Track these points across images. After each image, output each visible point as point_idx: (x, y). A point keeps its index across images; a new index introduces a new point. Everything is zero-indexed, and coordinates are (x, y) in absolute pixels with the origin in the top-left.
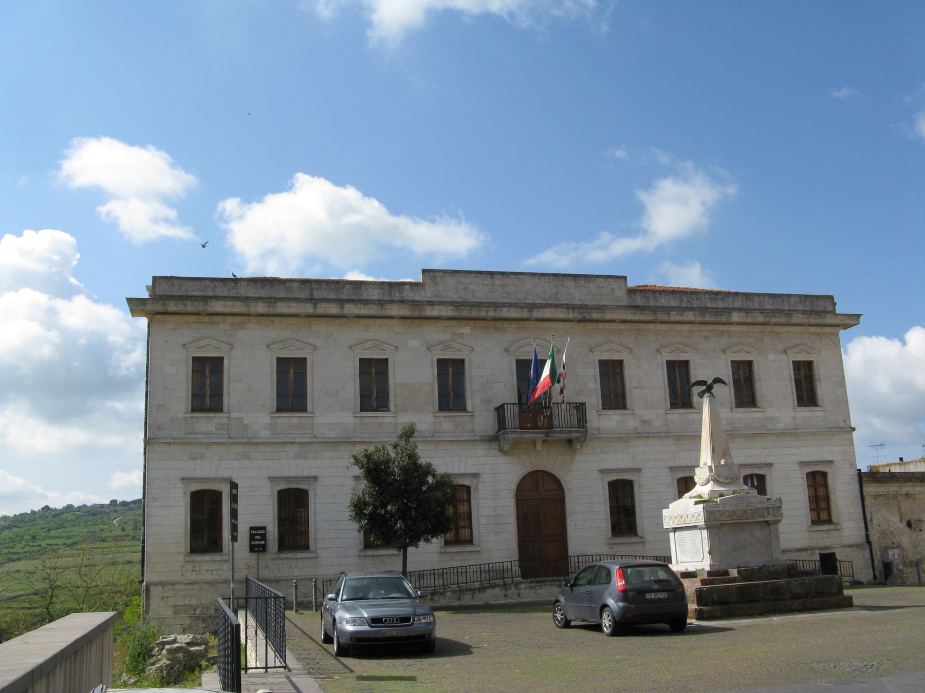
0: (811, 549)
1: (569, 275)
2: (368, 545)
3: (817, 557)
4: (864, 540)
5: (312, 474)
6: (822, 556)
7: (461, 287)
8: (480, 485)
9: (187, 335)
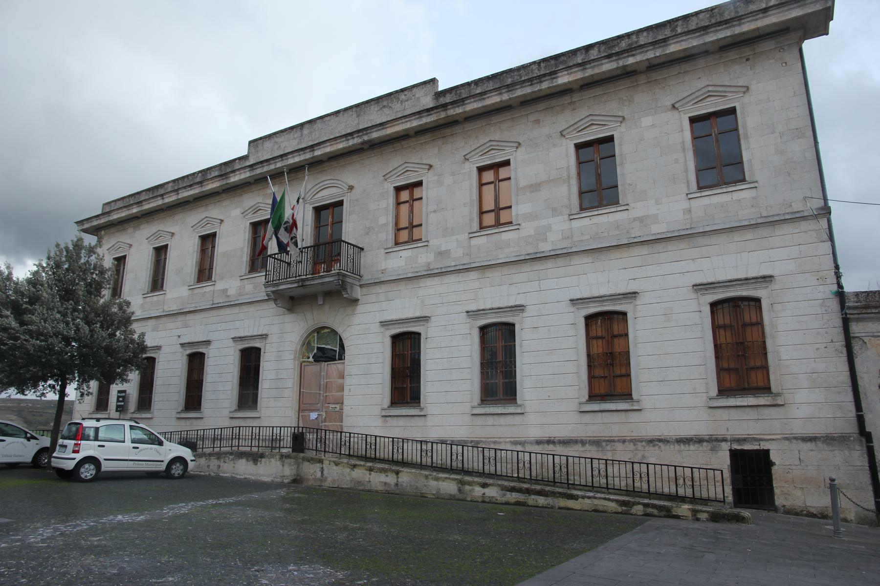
0: (714, 441)
1: (372, 100)
2: (724, 391)
3: (723, 460)
4: (851, 428)
5: (264, 333)
6: (736, 456)
7: (276, 147)
8: (268, 346)
9: (564, 120)
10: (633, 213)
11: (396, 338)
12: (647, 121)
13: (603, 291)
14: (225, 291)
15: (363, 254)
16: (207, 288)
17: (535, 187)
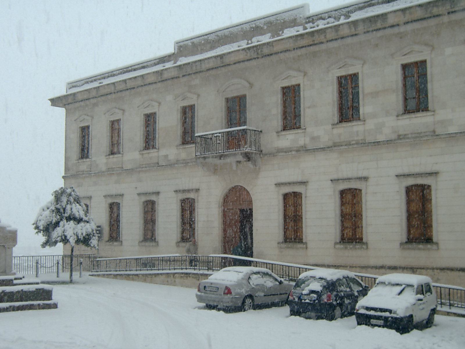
10: (438, 118)
11: (286, 196)
12: (448, 51)
13: (417, 170)
14: (166, 156)
15: (261, 135)
16: (153, 153)
17: (375, 94)
